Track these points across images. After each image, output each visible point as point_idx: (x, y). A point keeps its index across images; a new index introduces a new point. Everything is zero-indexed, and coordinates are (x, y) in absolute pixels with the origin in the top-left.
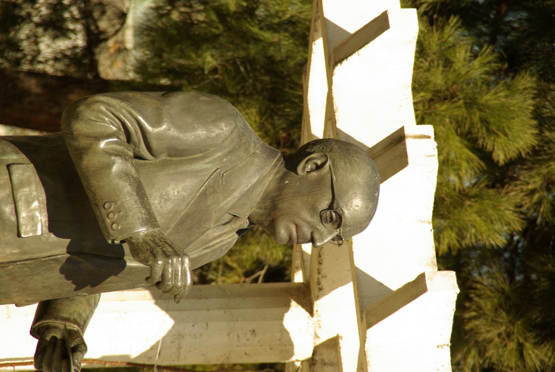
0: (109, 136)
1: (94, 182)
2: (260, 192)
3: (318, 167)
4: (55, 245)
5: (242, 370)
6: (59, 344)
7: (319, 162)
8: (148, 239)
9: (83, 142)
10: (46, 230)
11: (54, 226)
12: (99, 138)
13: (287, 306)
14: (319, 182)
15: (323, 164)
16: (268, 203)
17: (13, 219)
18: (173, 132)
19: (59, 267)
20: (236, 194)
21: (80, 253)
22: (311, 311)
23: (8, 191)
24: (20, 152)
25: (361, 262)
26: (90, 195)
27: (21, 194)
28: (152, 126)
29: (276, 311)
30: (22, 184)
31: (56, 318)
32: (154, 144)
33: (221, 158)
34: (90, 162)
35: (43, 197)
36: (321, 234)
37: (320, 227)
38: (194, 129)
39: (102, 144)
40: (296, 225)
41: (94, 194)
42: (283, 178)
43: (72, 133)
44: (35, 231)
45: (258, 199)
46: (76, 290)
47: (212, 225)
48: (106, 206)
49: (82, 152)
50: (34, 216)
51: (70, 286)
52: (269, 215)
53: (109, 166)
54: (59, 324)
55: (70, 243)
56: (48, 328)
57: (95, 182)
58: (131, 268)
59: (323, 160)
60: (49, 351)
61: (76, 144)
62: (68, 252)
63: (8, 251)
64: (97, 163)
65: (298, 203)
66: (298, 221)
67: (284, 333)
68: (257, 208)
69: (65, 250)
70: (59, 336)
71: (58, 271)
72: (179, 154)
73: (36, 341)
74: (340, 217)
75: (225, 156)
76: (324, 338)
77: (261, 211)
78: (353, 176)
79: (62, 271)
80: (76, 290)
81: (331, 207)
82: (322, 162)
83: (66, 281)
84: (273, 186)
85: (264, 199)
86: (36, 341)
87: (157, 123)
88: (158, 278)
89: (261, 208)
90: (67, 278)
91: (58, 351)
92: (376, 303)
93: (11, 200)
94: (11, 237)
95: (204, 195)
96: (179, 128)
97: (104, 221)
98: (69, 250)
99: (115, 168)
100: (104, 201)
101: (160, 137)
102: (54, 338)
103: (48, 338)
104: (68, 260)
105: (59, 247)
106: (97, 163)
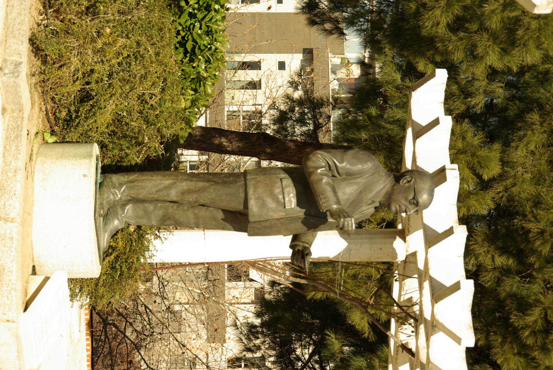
1: (315, 186)
3: (409, 182)
6: (301, 252)
10: (296, 205)
11: (299, 204)
13: (395, 238)
14: (409, 188)
15: (411, 180)
16: (387, 196)
17: (283, 201)
18: (348, 166)
19: (300, 221)
20: (374, 192)
21: (310, 215)
22: (405, 240)
23: (281, 189)
25: (426, 221)
27: (286, 190)
28: (340, 163)
30: (286, 187)
31: (300, 241)
32: (340, 171)
33: (368, 177)
34: (314, 178)
35: (295, 192)
38: (357, 165)
39: (319, 171)
41: (315, 191)
44: (291, 206)
45: (383, 194)
49: (311, 174)
51: (305, 228)
53: (322, 180)
54: (301, 244)
56: (296, 245)
58: (330, 222)
60: (297, 255)
63: (280, 214)
66: (400, 204)
67: (394, 249)
72: (350, 175)
74: (418, 203)
75: (370, 176)
76: (410, 252)
79: (302, 222)
81: (414, 198)
84: (390, 189)
85: (386, 194)
88: (341, 226)
90: (304, 225)
92: (432, 238)
93: (282, 193)
94: (281, 208)
95: (361, 192)
97: (319, 202)
99: (324, 181)
101: (343, 168)
102: (299, 250)
103: (296, 250)
104: (305, 218)
105: (301, 213)
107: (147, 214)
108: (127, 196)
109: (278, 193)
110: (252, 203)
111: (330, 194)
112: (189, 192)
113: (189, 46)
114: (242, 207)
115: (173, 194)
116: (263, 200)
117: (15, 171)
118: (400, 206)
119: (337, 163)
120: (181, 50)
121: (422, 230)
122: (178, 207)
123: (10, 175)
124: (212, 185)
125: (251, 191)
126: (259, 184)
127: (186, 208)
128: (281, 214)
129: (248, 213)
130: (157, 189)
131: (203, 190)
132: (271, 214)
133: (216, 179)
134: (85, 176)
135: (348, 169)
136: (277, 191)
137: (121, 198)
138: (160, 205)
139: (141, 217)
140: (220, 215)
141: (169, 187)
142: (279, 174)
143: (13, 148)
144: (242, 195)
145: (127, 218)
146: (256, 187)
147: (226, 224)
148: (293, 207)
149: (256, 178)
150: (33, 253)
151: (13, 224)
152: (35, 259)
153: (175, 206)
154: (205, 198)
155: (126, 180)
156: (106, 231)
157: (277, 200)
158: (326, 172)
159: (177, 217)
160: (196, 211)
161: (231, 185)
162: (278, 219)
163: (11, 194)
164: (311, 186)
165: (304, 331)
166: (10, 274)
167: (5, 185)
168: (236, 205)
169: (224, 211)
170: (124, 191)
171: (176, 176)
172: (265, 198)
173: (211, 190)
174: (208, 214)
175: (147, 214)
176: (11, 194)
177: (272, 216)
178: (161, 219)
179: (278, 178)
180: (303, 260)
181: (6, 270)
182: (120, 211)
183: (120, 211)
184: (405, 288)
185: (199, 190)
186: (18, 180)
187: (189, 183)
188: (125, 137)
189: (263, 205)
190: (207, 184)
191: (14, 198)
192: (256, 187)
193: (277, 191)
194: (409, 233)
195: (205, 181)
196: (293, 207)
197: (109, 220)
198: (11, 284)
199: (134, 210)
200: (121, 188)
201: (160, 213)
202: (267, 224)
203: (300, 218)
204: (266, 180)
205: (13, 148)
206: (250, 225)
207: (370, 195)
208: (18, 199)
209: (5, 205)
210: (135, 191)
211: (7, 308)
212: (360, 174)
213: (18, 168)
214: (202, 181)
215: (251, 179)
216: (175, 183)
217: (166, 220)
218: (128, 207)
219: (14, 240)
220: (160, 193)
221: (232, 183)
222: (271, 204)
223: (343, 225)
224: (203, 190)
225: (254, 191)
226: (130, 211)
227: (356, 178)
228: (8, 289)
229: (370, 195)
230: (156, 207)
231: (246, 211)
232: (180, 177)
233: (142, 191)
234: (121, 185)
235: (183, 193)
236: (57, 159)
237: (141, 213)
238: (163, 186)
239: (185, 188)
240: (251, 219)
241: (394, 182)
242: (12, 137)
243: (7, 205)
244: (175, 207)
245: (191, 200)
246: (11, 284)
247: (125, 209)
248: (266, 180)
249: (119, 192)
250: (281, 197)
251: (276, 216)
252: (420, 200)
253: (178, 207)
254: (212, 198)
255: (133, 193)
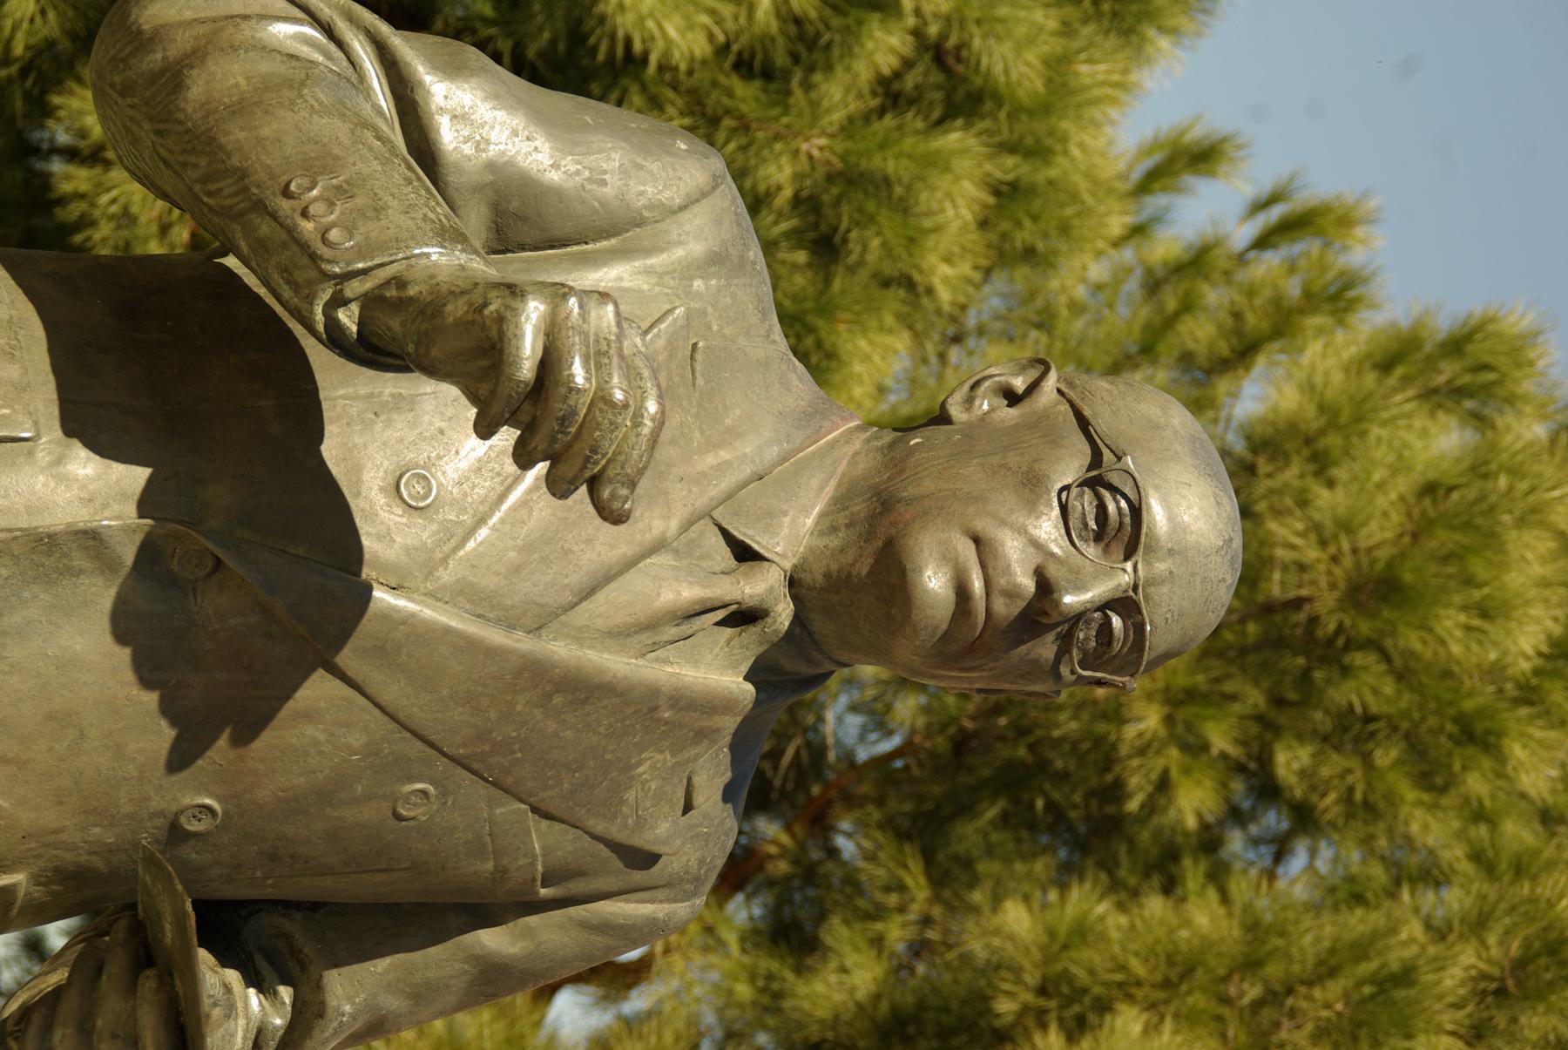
15: (1033, 387)
40: (977, 541)
48: (293, 187)
52: (869, 536)
55: (150, 481)
57: (241, 135)
59: (1034, 374)
62: (142, 514)
64: (243, 82)
68: (822, 533)
69: (131, 509)
71: (105, 623)
77: (835, 542)
82: (1029, 381)
83: (136, 691)
89: (834, 529)
98: (147, 503)
100: (284, 179)
106: (243, 82)
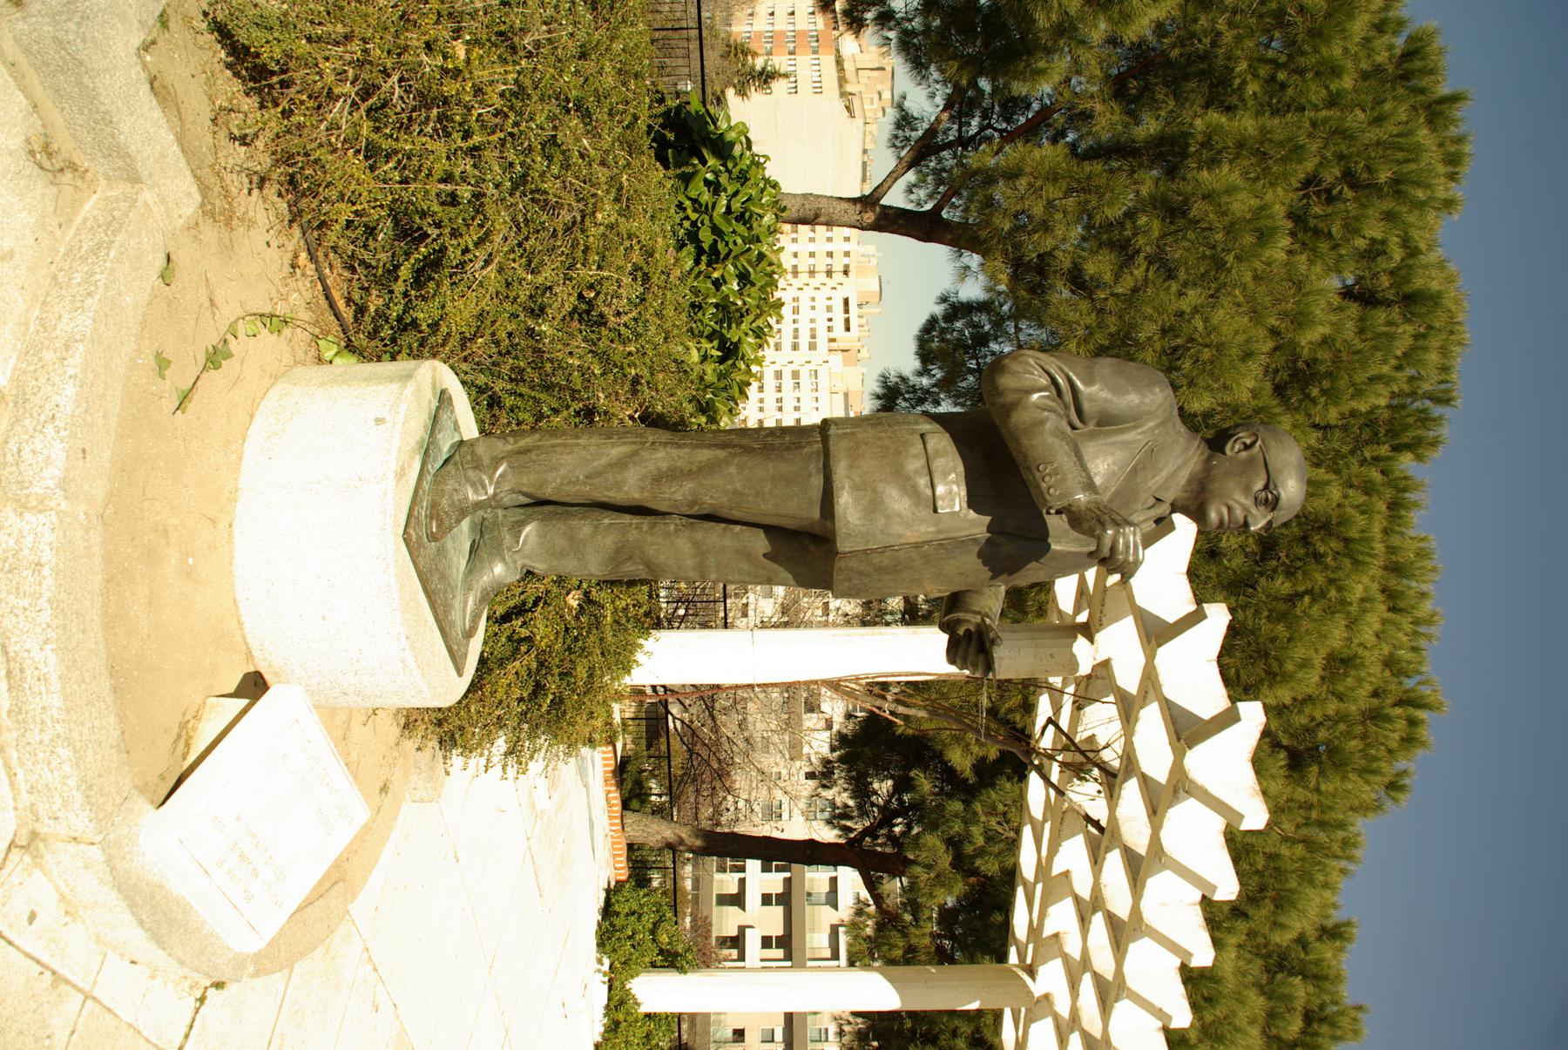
0: (1040, 390)
1: (1024, 441)
2: (1183, 477)
3: (1247, 447)
4: (973, 523)
5: (184, 735)
6: (975, 636)
7: (1248, 442)
8: (1092, 506)
9: (1011, 397)
10: (965, 505)
11: (972, 503)
12: (1029, 391)
13: (1076, 638)
14: (1251, 461)
15: (1253, 444)
16: (1194, 486)
17: (929, 492)
18: (1105, 394)
19: (977, 549)
20: (1164, 474)
21: (1001, 533)
22: (1092, 641)
23: (923, 461)
24: (808, 945)
25: (1142, 600)
26: (1019, 459)
27: (938, 464)
28: (1086, 384)
29: (1067, 641)
30: (938, 454)
31: (967, 611)
32: (1086, 406)
33: (1153, 429)
34: (1020, 418)
35: (961, 469)
36: (1255, 517)
37: (1254, 511)
38: (1128, 392)
39: (1035, 396)
41: (1025, 456)
42: (1209, 459)
43: (997, 389)
44: (953, 506)
45: (1183, 482)
46: (992, 578)
47: (1139, 507)
49: (1008, 410)
50: (952, 492)
51: (986, 573)
53: (1042, 422)
54: (969, 616)
56: (959, 622)
58: (1057, 552)
60: (964, 643)
61: (1001, 400)
63: (923, 529)
65: (1231, 484)
66: (1231, 503)
67: (1073, 656)
70: (972, 628)
72: (1108, 422)
73: (946, 637)
74: (1277, 499)
75: (1157, 427)
76: (1099, 660)
78: (1286, 455)
79: (980, 555)
80: (992, 578)
81: (1266, 487)
84: (1199, 467)
85: (1189, 482)
86: (946, 637)
87: (1089, 382)
88: (1106, 552)
90: (985, 564)
91: (974, 643)
92: (1156, 633)
93: (926, 471)
94: (926, 513)
95: (1134, 471)
96: (1116, 391)
97: (1038, 486)
99: (1048, 426)
101: (1092, 399)
102: (968, 631)
103: (961, 632)
104: (988, 541)
105: (977, 525)
107: (575, 546)
108: (513, 491)
109: (916, 471)
110: (845, 500)
111: (1065, 460)
112: (674, 475)
113: (706, 236)
114: (816, 514)
115: (631, 488)
116: (875, 491)
117: (67, 347)
118: (1229, 509)
119: (1079, 383)
120: (690, 248)
121: (1131, 618)
122: (653, 526)
123: (49, 356)
124: (735, 455)
125: (840, 469)
126: (864, 447)
127: (672, 527)
128: (924, 530)
129: (833, 532)
130: (589, 469)
131: (710, 468)
132: (897, 529)
133: (744, 441)
134: (379, 421)
135: (1106, 400)
136: (914, 464)
137: (495, 495)
138: (606, 521)
139: (562, 554)
140: (760, 543)
141: (621, 464)
142: (916, 423)
143: (78, 277)
144: (817, 482)
145: (525, 557)
146: (854, 457)
147: (775, 566)
148: (957, 508)
149: (853, 434)
150: (244, 638)
151: (41, 516)
152: (255, 654)
153: (645, 522)
154: (714, 494)
155: (510, 447)
156: (470, 589)
157: (914, 492)
158: (1052, 404)
159: (650, 551)
160: (699, 535)
161: (786, 455)
162: (917, 546)
163: (43, 418)
164: (1011, 444)
165: (882, 770)
166: (43, 689)
167: (29, 391)
168: (800, 508)
169: (771, 530)
170: (502, 476)
171: (639, 436)
172: (880, 487)
173: (733, 470)
174: (727, 542)
175: (575, 546)
176: (43, 418)
177: (900, 536)
178: (612, 559)
179: (913, 432)
180: (981, 657)
181: (28, 673)
182: (508, 539)
183: (508, 539)
184: (1085, 720)
185: (700, 469)
186: (71, 371)
187: (674, 452)
188: (548, 387)
189: (874, 506)
190: (721, 454)
191: (50, 429)
192: (854, 457)
193: (914, 464)
194: (1101, 626)
195: (717, 446)
196: (957, 508)
197: (481, 561)
198: (49, 722)
199: (542, 536)
200: (496, 469)
201: (609, 541)
202: (885, 560)
203: (975, 540)
204: (880, 439)
205: (78, 277)
206: (840, 563)
207: (1154, 483)
208: (62, 433)
209: (20, 451)
210: (533, 476)
211: (58, 800)
212: (1131, 420)
213: (78, 337)
214: (709, 446)
215: (839, 436)
216: (635, 453)
217: (623, 562)
218: (528, 529)
219: (46, 571)
220: (595, 481)
221: (788, 449)
222: (897, 502)
223: (1113, 549)
224: (710, 468)
225: (851, 467)
226: (533, 540)
227: (1123, 431)
228: (46, 738)
229: (1154, 483)
230: (596, 527)
231: (829, 525)
232: (651, 439)
233: (549, 476)
234: (496, 462)
235: (658, 478)
236: (322, 384)
237: (561, 542)
238: (604, 461)
239: (664, 465)
240: (843, 545)
241: (1208, 452)
242: (85, 248)
243: (26, 454)
244: (645, 528)
245: (679, 497)
246: (49, 722)
247: (520, 532)
248: (880, 439)
249: (491, 479)
250: (923, 482)
251: (912, 535)
252: (1283, 494)
253: (653, 526)
254: (735, 492)
255: (529, 482)
